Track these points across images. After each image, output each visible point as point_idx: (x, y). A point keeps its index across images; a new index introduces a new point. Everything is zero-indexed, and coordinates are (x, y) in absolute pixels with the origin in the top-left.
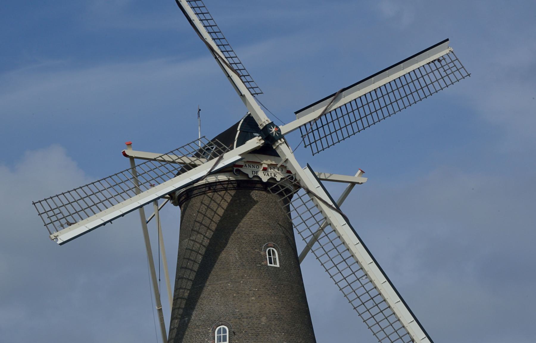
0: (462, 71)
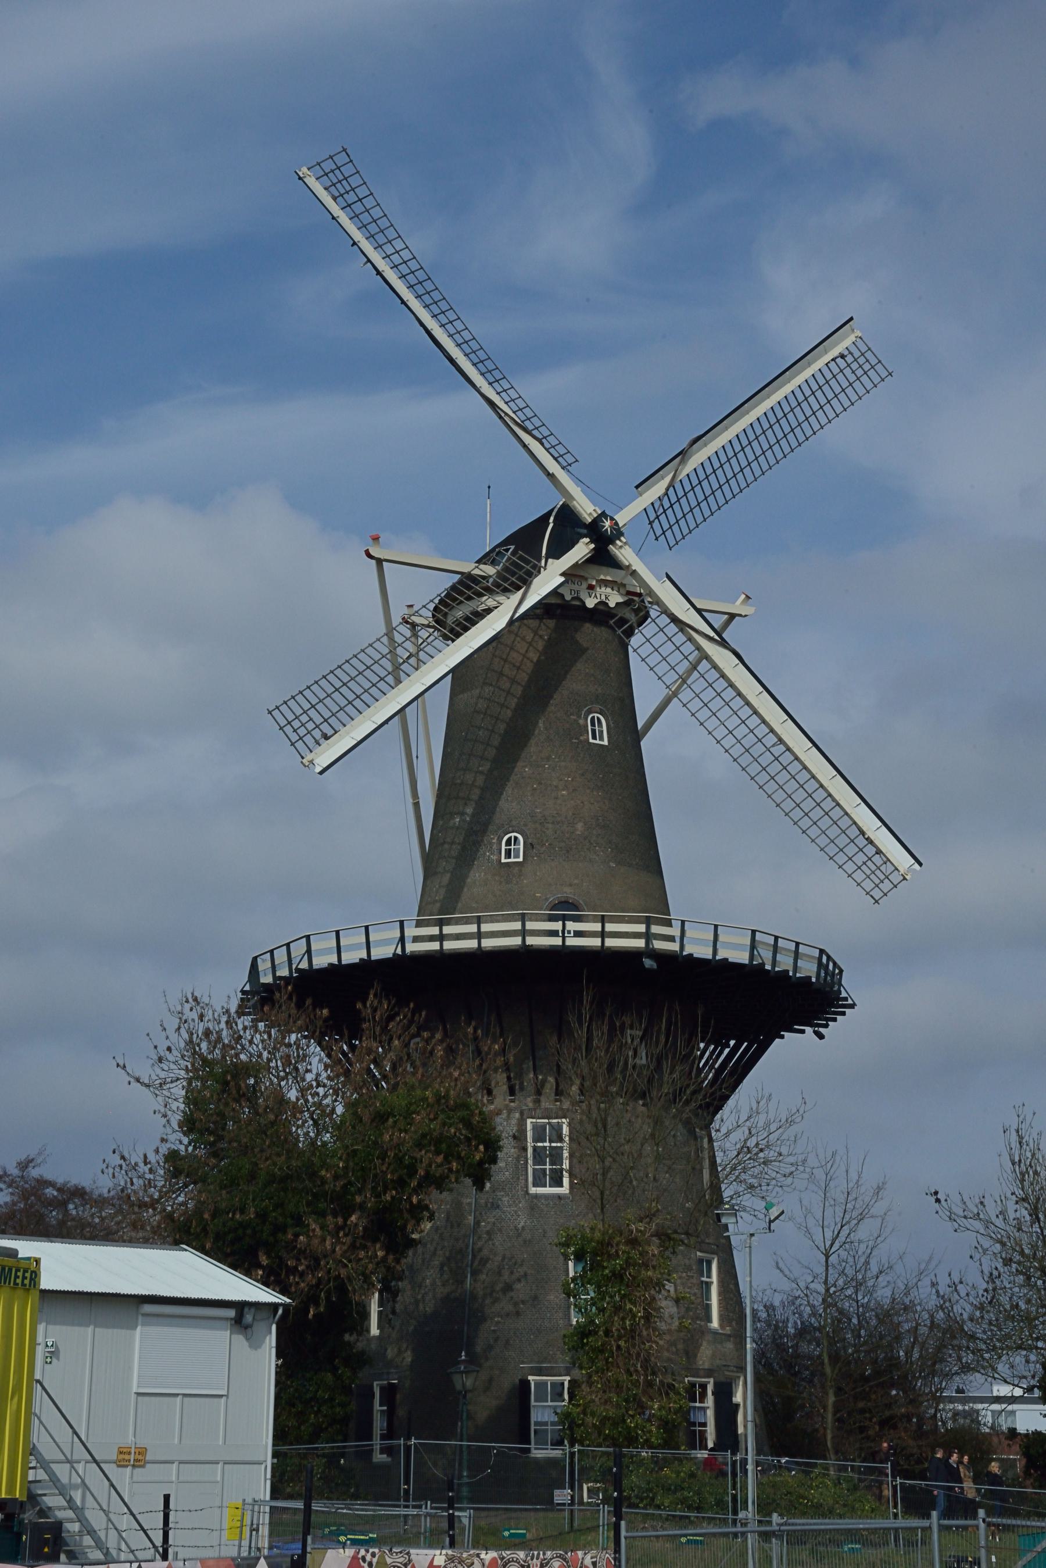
0: (879, 367)
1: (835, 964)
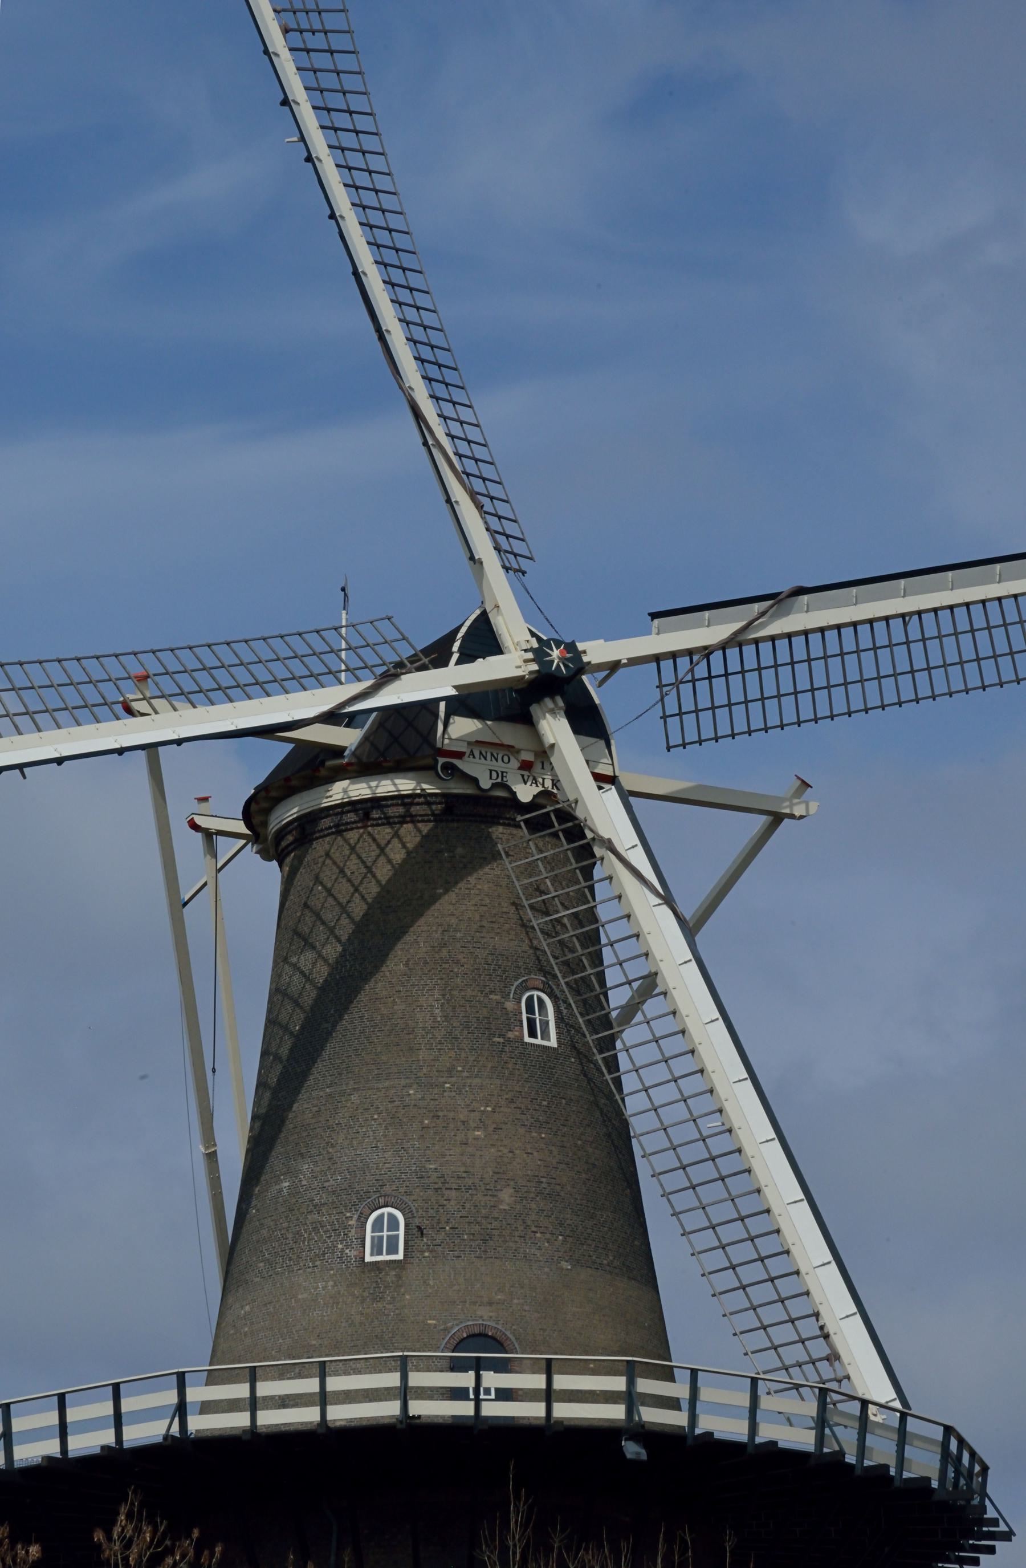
1: (973, 1454)
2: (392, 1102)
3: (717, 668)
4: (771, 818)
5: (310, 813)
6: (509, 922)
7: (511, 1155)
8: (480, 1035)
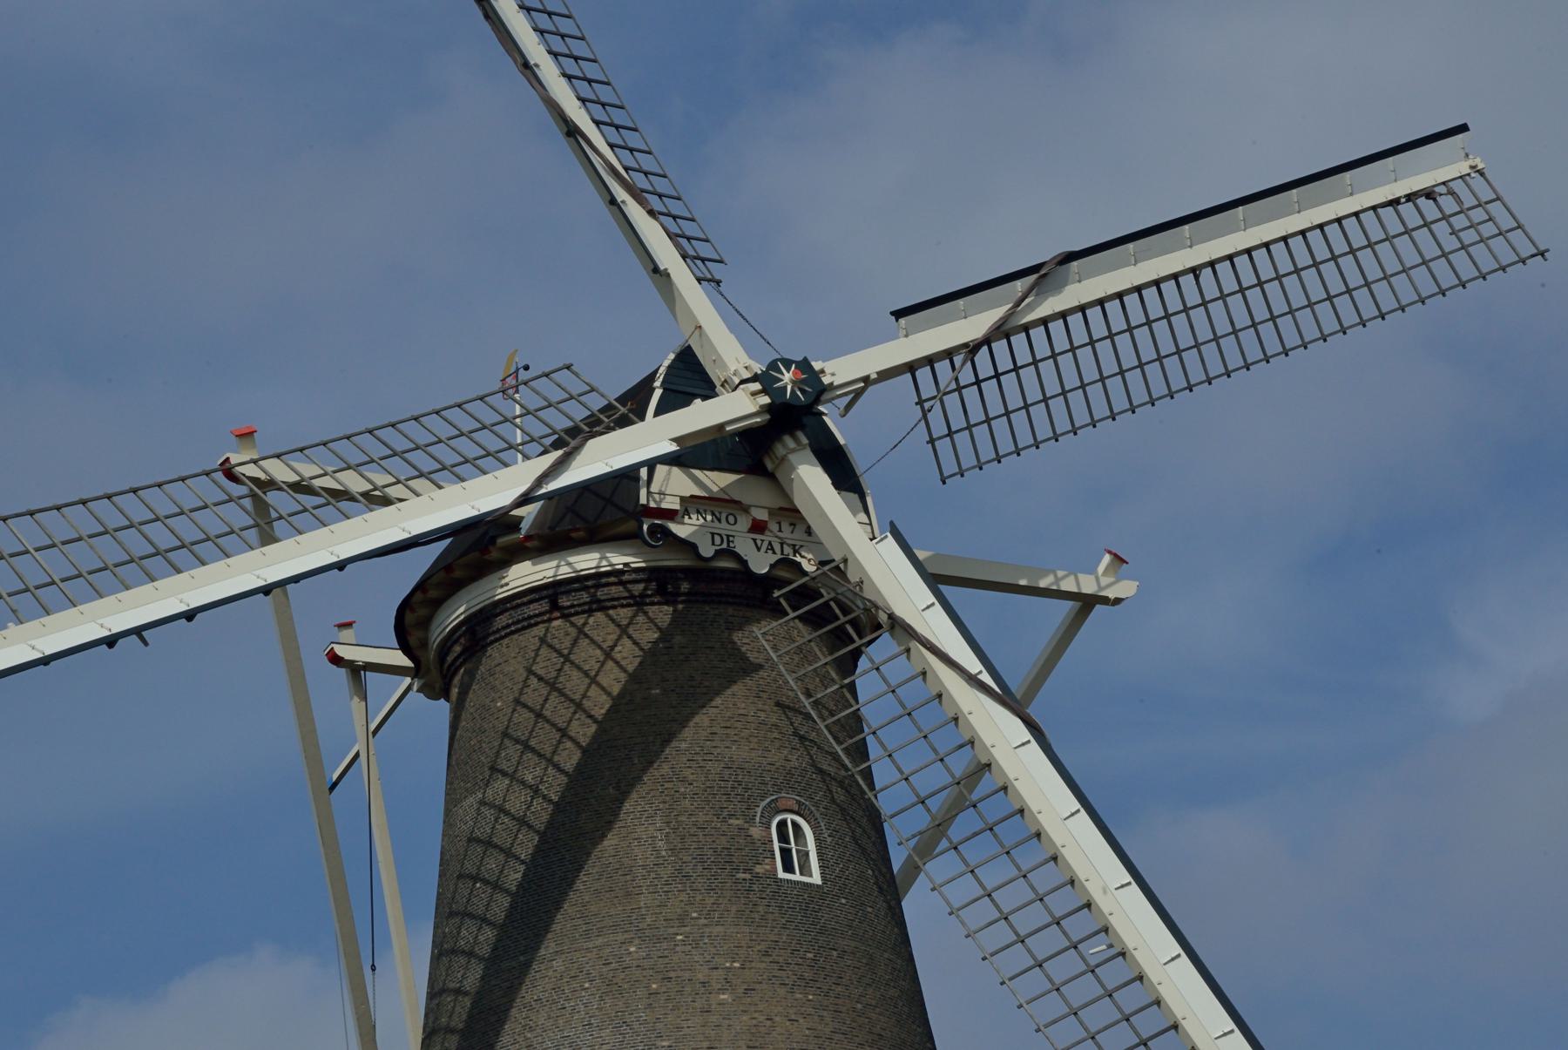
2: (608, 964)
3: (985, 369)
4: (1078, 605)
5: (481, 611)
6: (748, 727)
7: (769, 1023)
8: (719, 871)
